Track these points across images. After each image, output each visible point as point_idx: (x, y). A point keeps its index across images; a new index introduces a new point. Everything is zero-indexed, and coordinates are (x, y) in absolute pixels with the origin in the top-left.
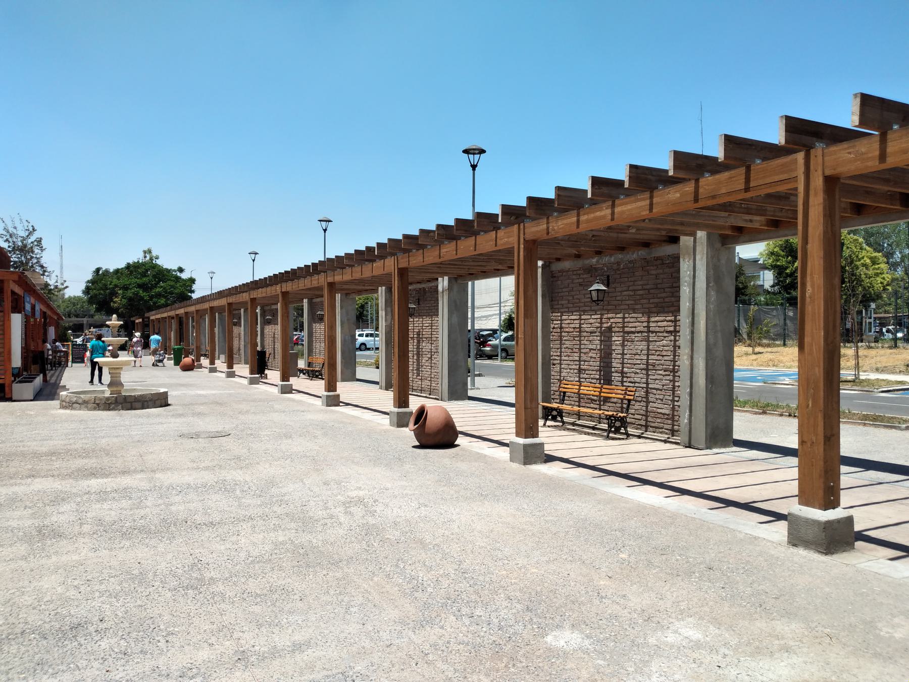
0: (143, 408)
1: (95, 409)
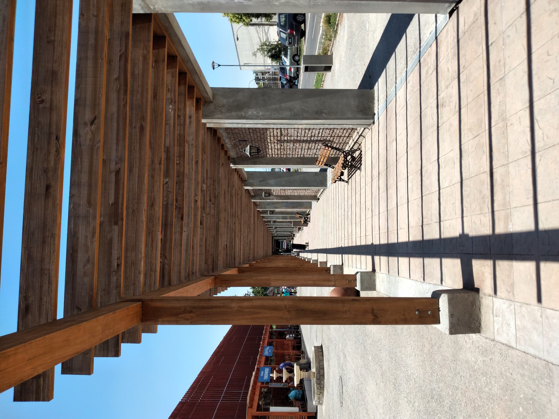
0: (323, 369)
1: (323, 395)
